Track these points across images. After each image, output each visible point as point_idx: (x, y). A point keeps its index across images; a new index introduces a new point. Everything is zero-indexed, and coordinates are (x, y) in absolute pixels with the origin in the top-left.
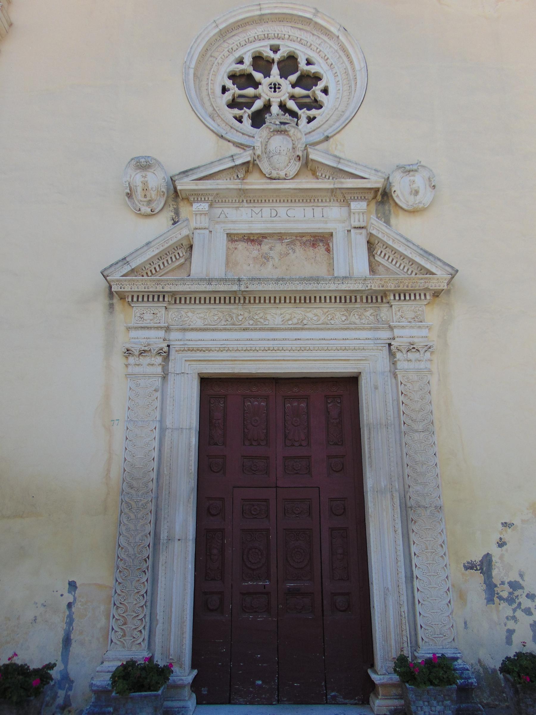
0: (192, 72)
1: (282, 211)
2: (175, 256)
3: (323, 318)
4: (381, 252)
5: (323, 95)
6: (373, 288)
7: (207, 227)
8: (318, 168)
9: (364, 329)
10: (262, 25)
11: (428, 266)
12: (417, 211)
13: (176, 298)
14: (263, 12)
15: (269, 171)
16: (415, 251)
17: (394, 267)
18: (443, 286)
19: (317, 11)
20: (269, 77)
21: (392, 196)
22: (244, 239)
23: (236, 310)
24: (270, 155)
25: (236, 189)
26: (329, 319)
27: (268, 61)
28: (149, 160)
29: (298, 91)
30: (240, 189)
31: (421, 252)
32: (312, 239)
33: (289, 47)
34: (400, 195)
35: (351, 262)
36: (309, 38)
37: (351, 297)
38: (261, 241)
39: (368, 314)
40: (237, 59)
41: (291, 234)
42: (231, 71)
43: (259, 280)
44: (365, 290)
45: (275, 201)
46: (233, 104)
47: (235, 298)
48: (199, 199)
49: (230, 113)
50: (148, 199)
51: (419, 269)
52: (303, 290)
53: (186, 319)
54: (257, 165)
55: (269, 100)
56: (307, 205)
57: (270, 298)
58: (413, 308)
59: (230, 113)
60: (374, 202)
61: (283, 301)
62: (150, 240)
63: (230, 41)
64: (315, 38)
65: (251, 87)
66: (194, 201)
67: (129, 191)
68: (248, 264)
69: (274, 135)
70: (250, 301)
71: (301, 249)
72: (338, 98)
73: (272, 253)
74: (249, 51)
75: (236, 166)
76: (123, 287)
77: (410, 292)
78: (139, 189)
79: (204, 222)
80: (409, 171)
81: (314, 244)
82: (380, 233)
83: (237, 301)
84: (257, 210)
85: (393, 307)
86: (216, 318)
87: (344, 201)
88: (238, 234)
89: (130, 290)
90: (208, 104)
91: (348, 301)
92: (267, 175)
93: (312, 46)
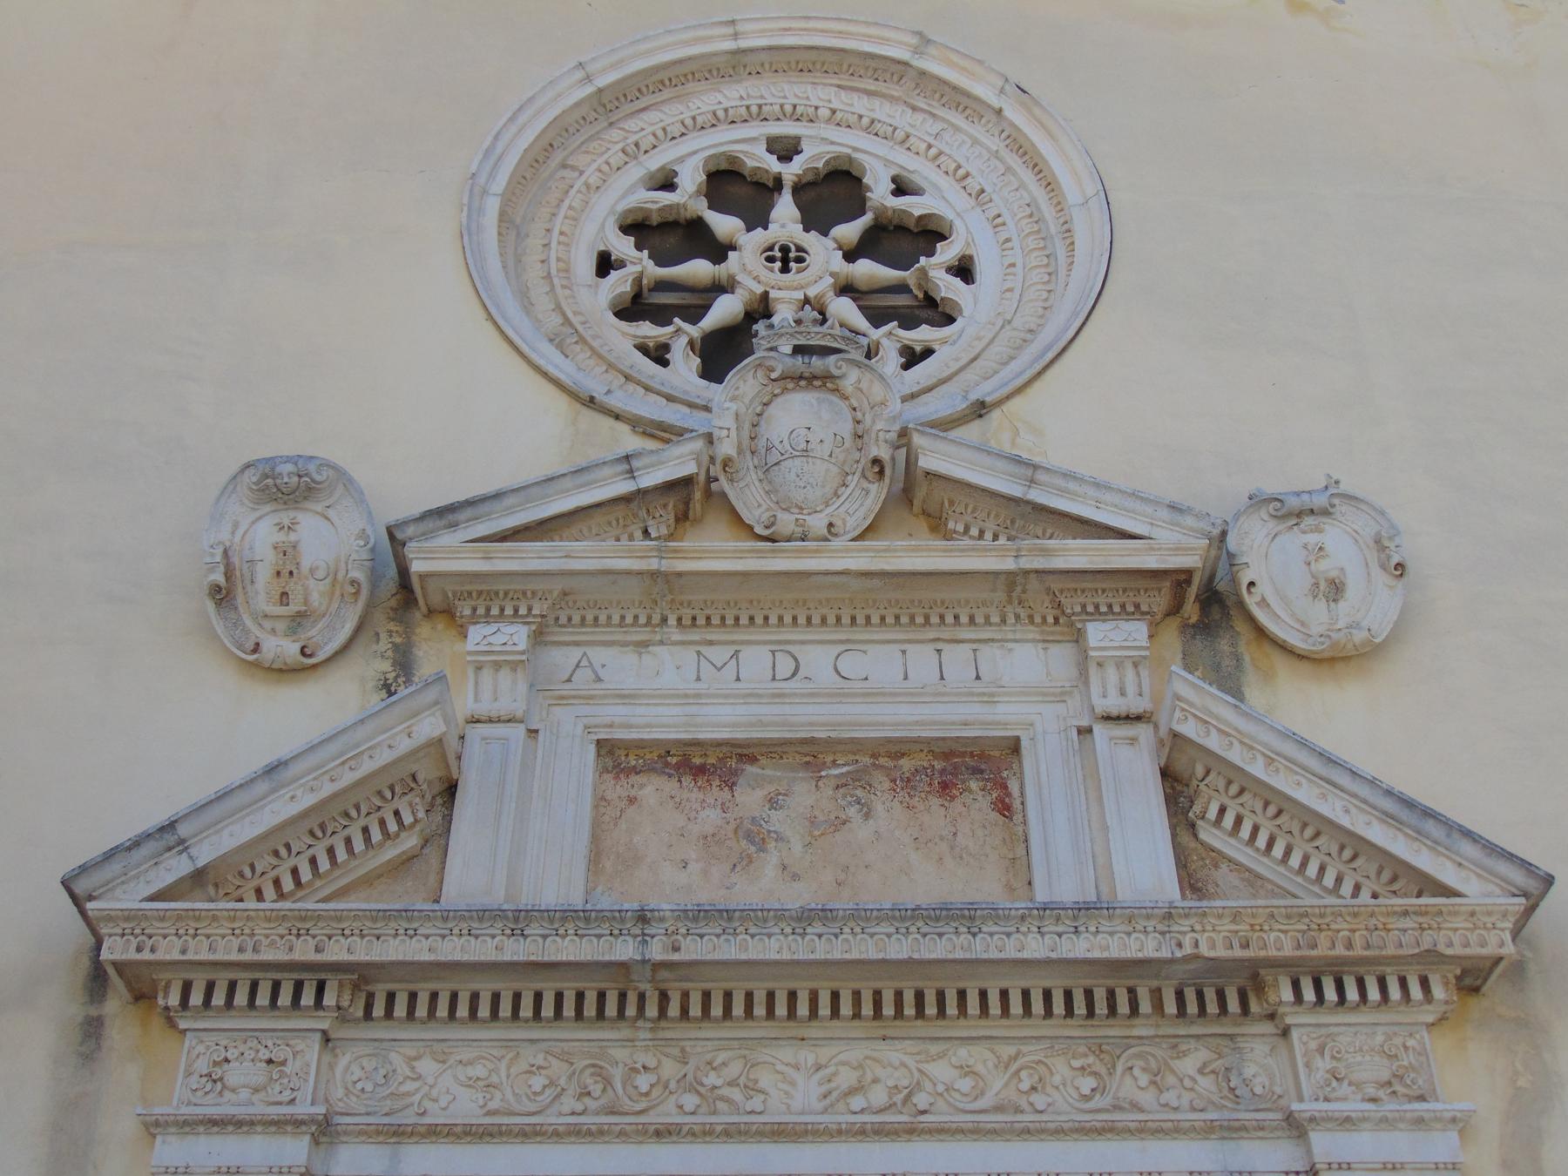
0: (493, 206)
1: (818, 659)
2: (382, 823)
3: (997, 1084)
4: (1222, 810)
5: (958, 282)
6: (1205, 950)
7: (519, 714)
8: (952, 503)
9: (1176, 1131)
10: (740, 82)
11: (1424, 861)
12: (1346, 659)
13: (370, 997)
14: (744, 44)
15: (767, 514)
16: (1365, 802)
17: (1281, 869)
18: (1498, 942)
19: (926, 41)
20: (766, 228)
21: (1241, 605)
22: (667, 764)
23: (625, 1050)
24: (772, 460)
25: (640, 573)
26: (1025, 1086)
27: (759, 185)
28: (312, 468)
29: (867, 270)
30: (654, 575)
31: (1388, 805)
32: (938, 765)
33: (832, 143)
34: (1271, 600)
35: (1104, 846)
36: (902, 118)
37: (1111, 994)
38: (735, 773)
39: (1188, 1065)
40: (651, 176)
41: (855, 746)
42: (630, 211)
43: (726, 917)
44: (1172, 961)
45: (788, 619)
46: (633, 308)
47: (623, 997)
48: (495, 611)
49: (624, 334)
50: (293, 608)
51: (1386, 876)
52: (909, 962)
53: (409, 1086)
54: (724, 495)
55: (765, 295)
56: (911, 636)
57: (771, 996)
58: (1380, 1039)
59: (624, 334)
60: (1173, 624)
61: (824, 1010)
62: (283, 752)
63: (632, 124)
64: (919, 117)
65: (703, 362)
66: (474, 619)
67: (221, 580)
68: (675, 855)
69: (785, 390)
70: (685, 1011)
71: (896, 804)
72: (1010, 290)
73: (777, 821)
74: (695, 153)
75: (641, 493)
76: (149, 943)
77: (1361, 970)
78: (263, 574)
79: (508, 693)
80: (1299, 514)
81: (945, 786)
82: (1214, 732)
83: (631, 1011)
84: (719, 654)
85: (1295, 1034)
86: (538, 1082)
87: (1056, 620)
88: (640, 745)
89: (176, 955)
90: (543, 304)
91: (1101, 1008)
92: (759, 530)
93: (912, 140)
